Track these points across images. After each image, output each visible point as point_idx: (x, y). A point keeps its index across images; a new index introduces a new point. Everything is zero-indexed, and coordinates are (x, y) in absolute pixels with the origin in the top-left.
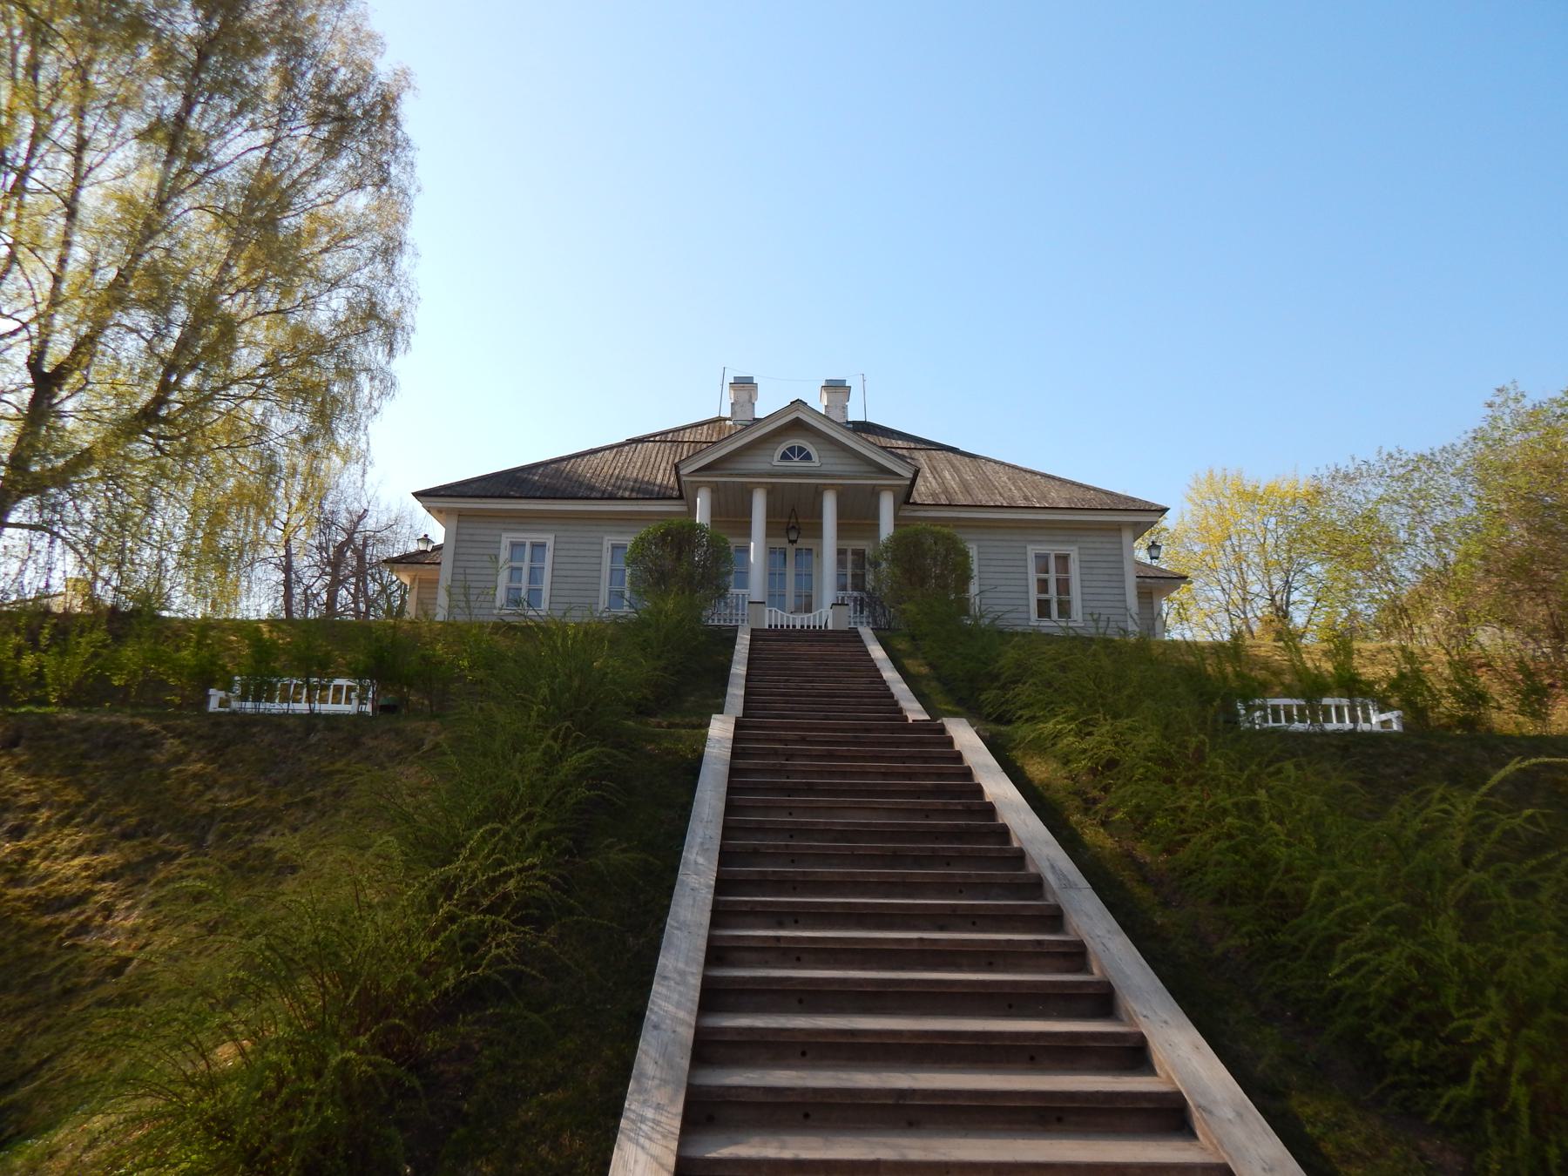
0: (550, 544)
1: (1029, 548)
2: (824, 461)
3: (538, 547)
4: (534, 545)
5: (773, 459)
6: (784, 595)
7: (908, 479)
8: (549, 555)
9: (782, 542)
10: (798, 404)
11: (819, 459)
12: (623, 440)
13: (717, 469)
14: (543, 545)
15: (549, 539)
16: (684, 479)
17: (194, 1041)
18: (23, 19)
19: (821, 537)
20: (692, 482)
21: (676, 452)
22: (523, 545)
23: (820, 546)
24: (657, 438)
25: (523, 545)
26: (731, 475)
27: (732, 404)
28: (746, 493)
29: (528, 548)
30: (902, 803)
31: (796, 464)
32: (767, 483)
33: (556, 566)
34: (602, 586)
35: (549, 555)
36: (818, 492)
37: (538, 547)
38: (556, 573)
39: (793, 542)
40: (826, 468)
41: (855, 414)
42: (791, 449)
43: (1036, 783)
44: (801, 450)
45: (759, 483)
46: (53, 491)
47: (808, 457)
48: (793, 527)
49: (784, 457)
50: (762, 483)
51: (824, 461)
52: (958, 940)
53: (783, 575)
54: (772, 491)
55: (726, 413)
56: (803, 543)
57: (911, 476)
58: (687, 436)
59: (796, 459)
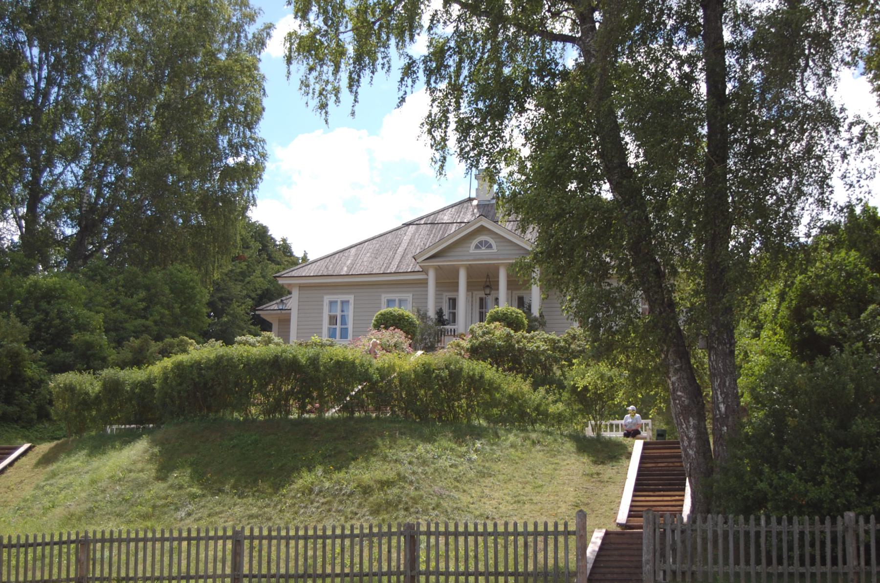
0: (352, 301)
3: (344, 303)
4: (343, 302)
8: (351, 307)
12: (400, 224)
13: (443, 256)
14: (348, 302)
15: (351, 298)
17: (598, 422)
18: (155, 379)
22: (336, 302)
24: (422, 222)
25: (336, 302)
29: (339, 304)
31: (484, 250)
34: (324, 326)
35: (351, 307)
37: (344, 303)
42: (481, 243)
43: (303, 361)
44: (486, 242)
46: (31, 99)
47: (490, 247)
49: (477, 247)
55: (473, 195)
58: (446, 218)
59: (483, 248)
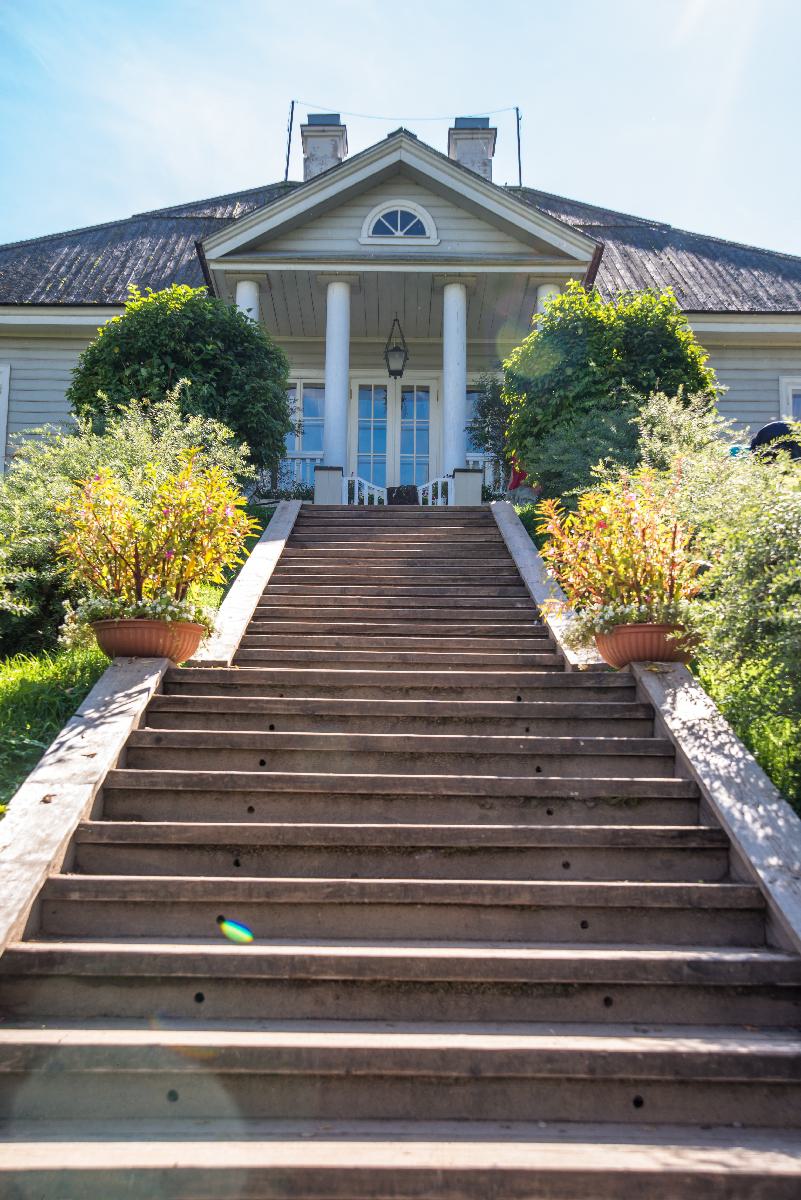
1: (785, 380)
2: (445, 235)
5: (356, 234)
6: (321, 387)
7: (584, 263)
9: (378, 377)
10: (402, 135)
11: (441, 232)
16: (213, 266)
19: (440, 366)
20: (226, 272)
21: (574, 720)
23: (439, 380)
26: (290, 260)
27: (306, 160)
28: (318, 286)
30: (395, 627)
31: (399, 241)
32: (349, 273)
33: (14, 396)
36: (436, 287)
38: (14, 407)
39: (396, 373)
40: (448, 249)
41: (503, 173)
42: (391, 217)
44: (407, 217)
45: (335, 274)
47: (418, 230)
48: (397, 349)
49: (379, 229)
50: (341, 273)
51: (445, 235)
52: (339, 1050)
53: (381, 431)
54: (358, 286)
56: (412, 377)
57: (589, 258)
59: (399, 233)
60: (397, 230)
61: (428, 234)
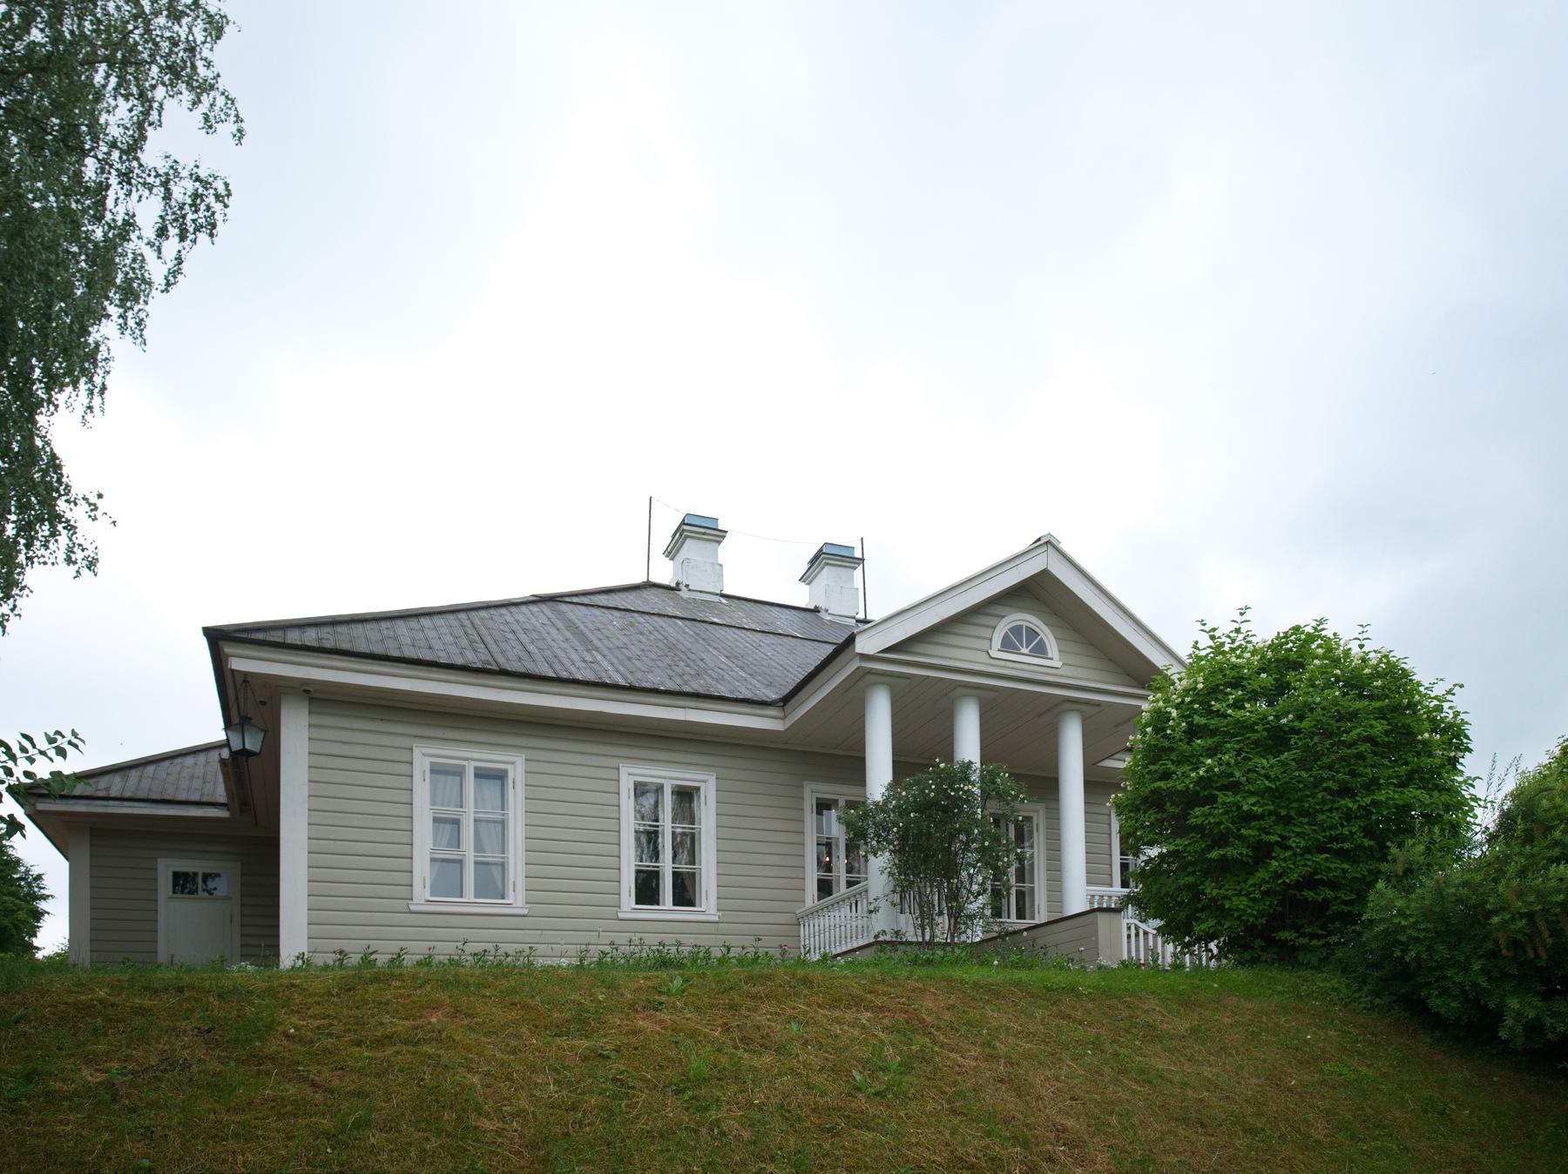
42: (1016, 630)
44: (1032, 634)
47: (1040, 650)
49: (1007, 645)
60: (1027, 647)
61: (1050, 655)
